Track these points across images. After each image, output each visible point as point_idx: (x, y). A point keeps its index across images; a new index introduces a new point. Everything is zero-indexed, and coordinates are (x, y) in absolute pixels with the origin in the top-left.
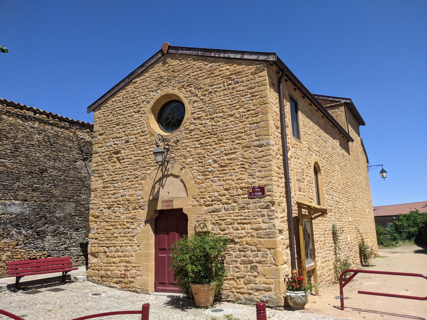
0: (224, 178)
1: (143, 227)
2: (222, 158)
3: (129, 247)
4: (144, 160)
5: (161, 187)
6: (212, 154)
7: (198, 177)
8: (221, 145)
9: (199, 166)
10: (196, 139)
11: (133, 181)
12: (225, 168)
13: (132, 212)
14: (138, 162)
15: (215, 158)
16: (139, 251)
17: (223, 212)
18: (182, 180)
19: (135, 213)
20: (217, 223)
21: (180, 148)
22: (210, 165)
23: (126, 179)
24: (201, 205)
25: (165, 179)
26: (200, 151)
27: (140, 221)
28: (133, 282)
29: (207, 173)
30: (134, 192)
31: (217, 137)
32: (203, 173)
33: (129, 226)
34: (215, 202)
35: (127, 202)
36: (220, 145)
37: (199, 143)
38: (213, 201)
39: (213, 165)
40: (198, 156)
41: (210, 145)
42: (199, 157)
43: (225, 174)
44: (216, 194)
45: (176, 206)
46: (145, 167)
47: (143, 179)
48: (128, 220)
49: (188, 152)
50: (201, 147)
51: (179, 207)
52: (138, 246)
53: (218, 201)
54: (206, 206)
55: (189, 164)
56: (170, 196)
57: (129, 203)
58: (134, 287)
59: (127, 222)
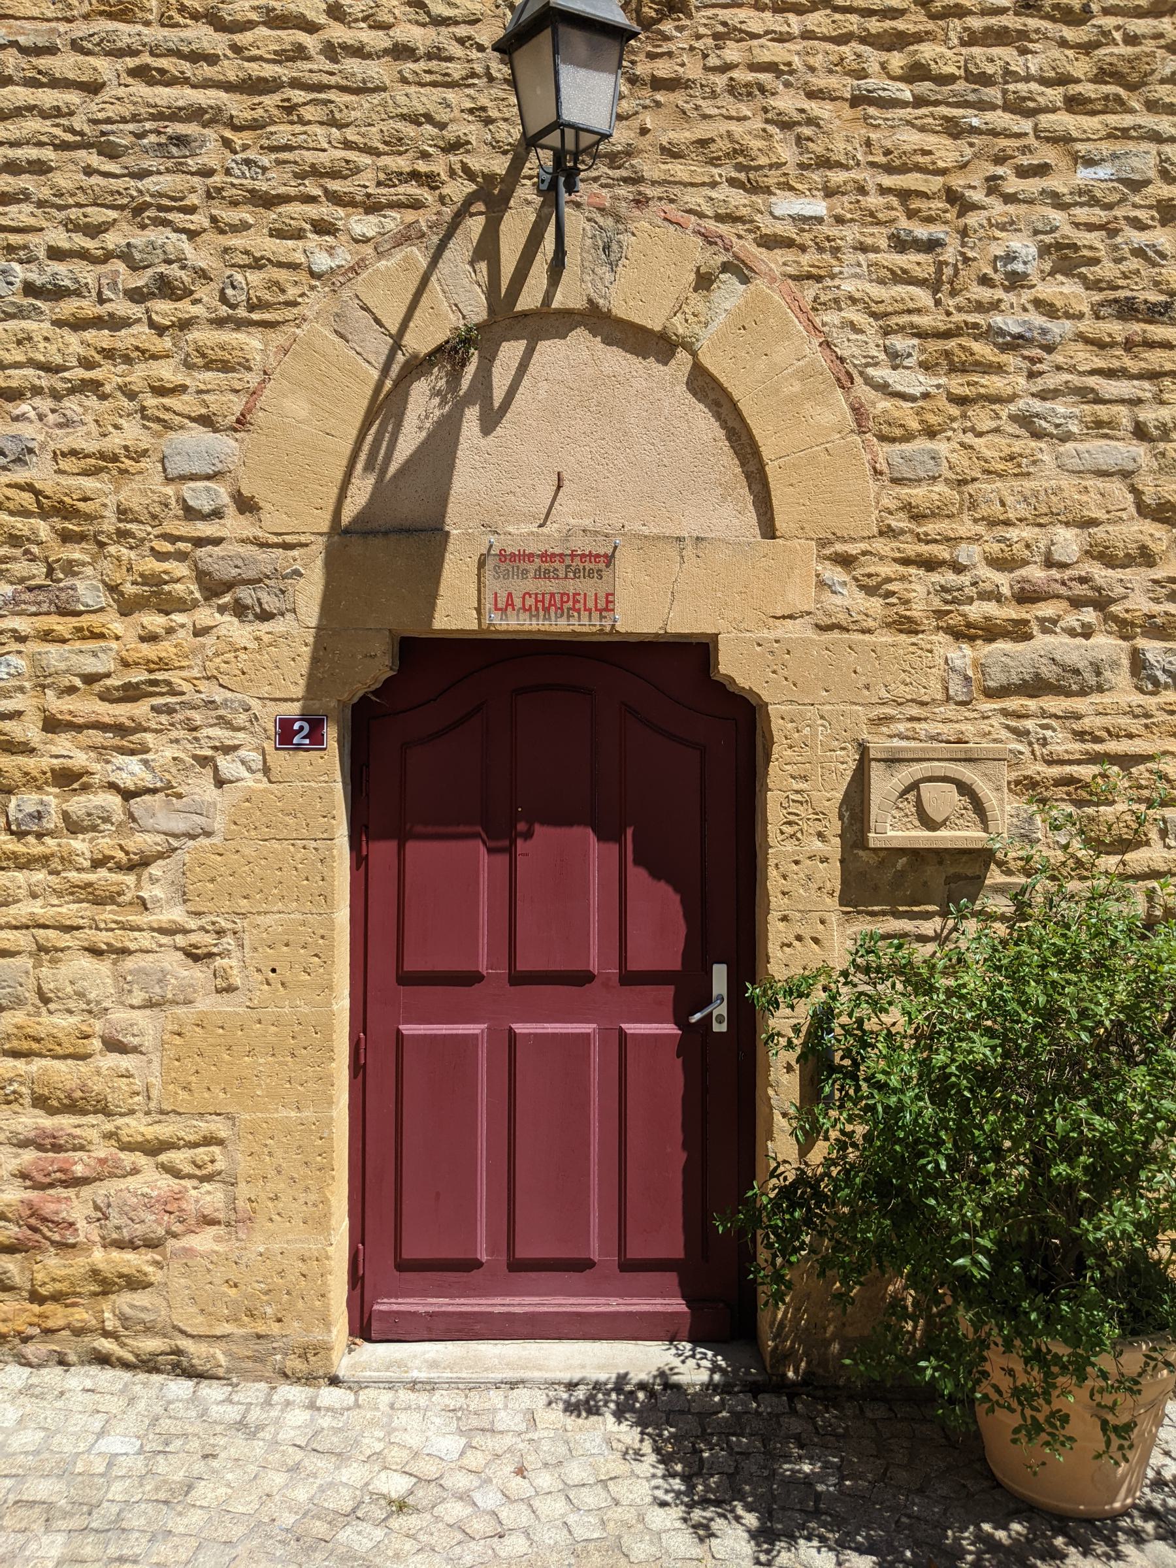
0: (1149, 415)
1: (252, 782)
2: (1139, 238)
3: (87, 962)
4: (255, 126)
5: (472, 414)
6: (1033, 185)
7: (881, 373)
8: (1128, 120)
9: (902, 277)
10: (875, 25)
11: (116, 323)
12: (1159, 332)
13: (117, 626)
14: (180, 141)
15: (1067, 229)
16: (207, 1003)
17: (1123, 692)
18: (706, 387)
19: (150, 638)
20: (1070, 781)
21: (693, 70)
22: (1016, 281)
23: (30, 289)
24: (907, 626)
25: (510, 352)
26: (911, 139)
27: (224, 722)
28: (135, 1283)
29: (977, 347)
30: (132, 433)
31: (1087, 48)
32: (934, 345)
33: (81, 760)
34: (1047, 610)
35: (43, 529)
36: (1113, 120)
37: (897, 61)
38: (1027, 596)
39: (1047, 290)
40: (888, 181)
41: (1016, 106)
42: (905, 195)
43: (1153, 376)
44: (1068, 542)
45: (642, 607)
46: (268, 201)
47: (257, 314)
48: (59, 706)
49: (786, 125)
50: (919, 102)
51: (684, 621)
52: (194, 955)
53: (1077, 603)
54: (958, 635)
55: (789, 243)
56: (572, 513)
57: (66, 537)
58: (149, 1330)
59: (52, 725)
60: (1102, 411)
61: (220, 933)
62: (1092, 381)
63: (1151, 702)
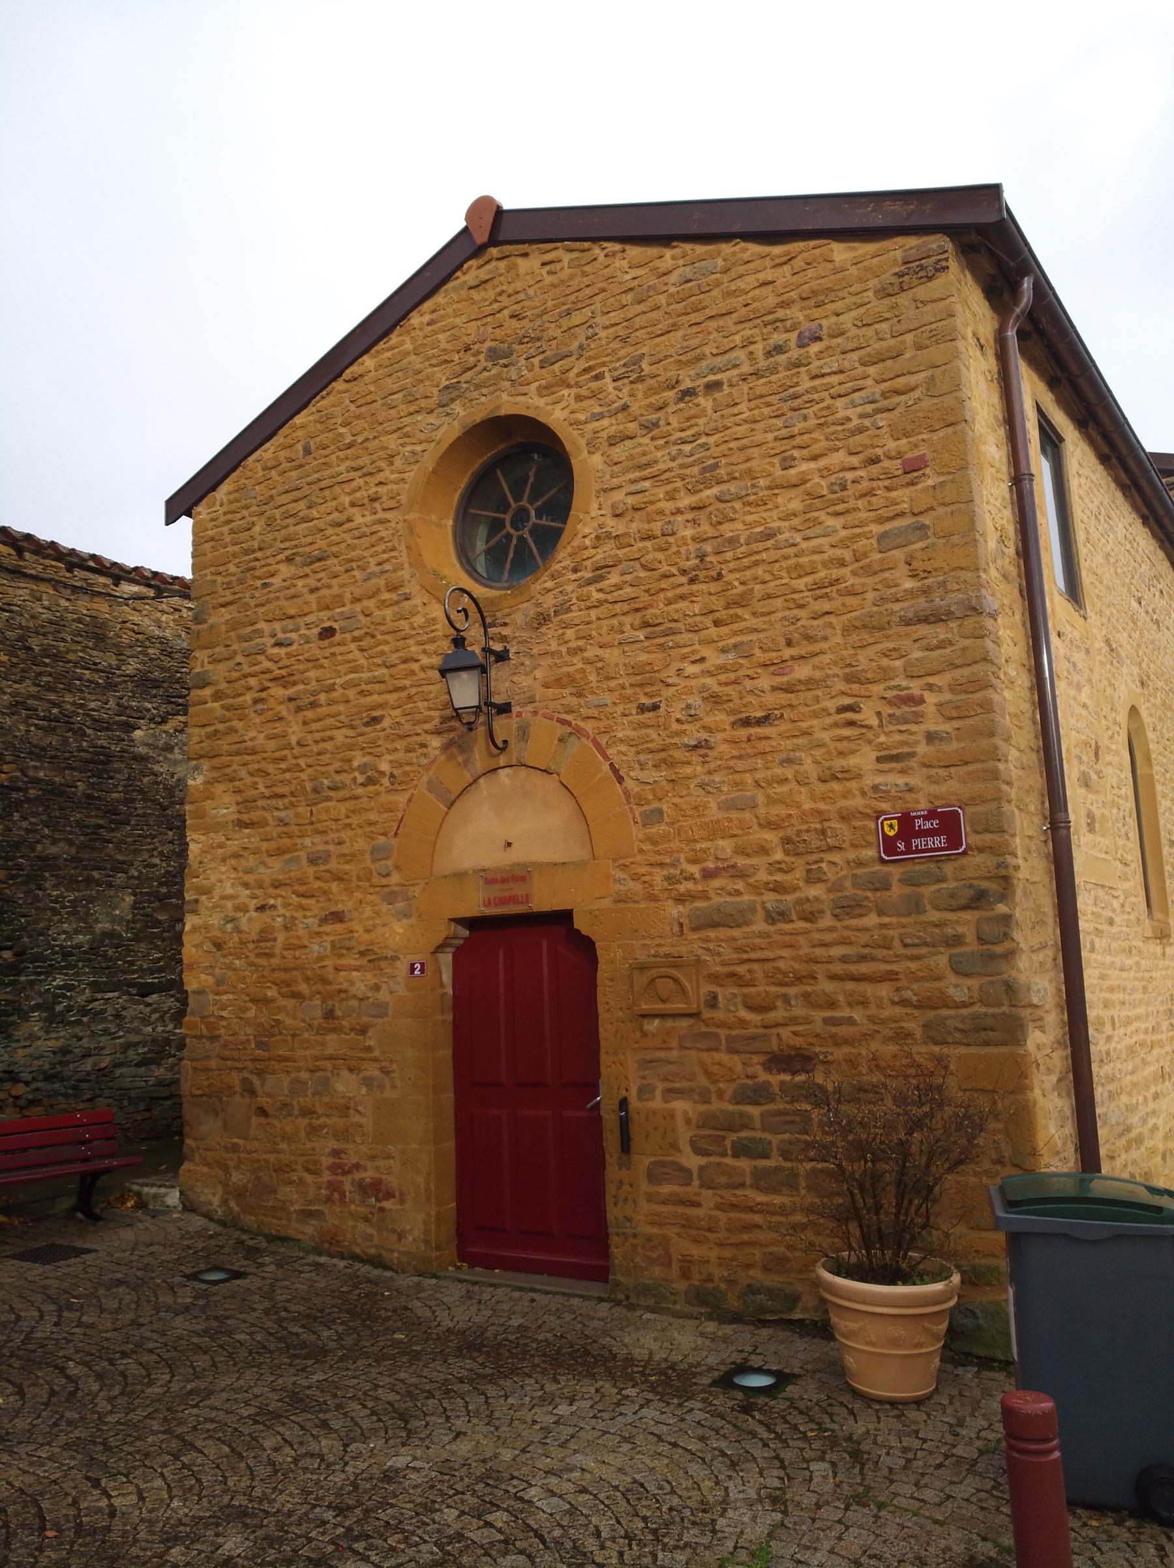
8: (743, 625)
36: (735, 627)
39: (708, 720)
44: (725, 846)
60: (737, 777)
61: (392, 1061)
62: (731, 763)
63: (772, 928)
